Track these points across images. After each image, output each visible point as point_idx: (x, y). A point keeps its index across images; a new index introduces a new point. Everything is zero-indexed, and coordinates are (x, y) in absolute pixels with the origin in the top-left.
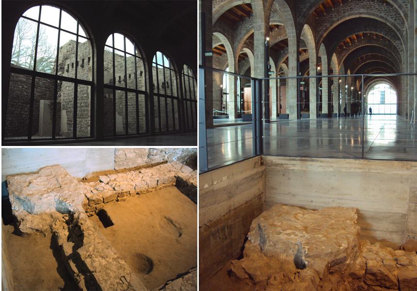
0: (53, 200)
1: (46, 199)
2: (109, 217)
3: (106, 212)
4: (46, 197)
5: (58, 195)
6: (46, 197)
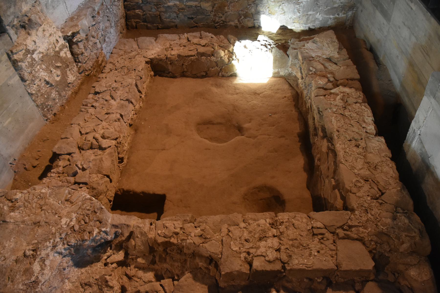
0: (58, 258)
1: (46, 272)
2: (143, 193)
3: (128, 192)
4: (42, 269)
5: (58, 239)
6: (42, 269)
